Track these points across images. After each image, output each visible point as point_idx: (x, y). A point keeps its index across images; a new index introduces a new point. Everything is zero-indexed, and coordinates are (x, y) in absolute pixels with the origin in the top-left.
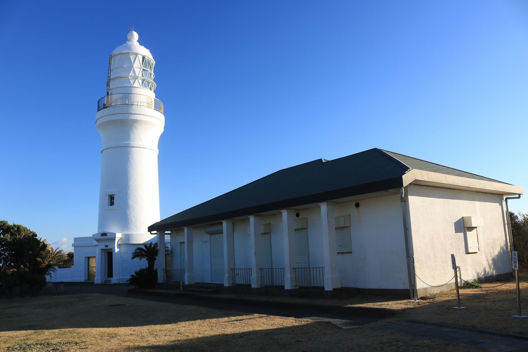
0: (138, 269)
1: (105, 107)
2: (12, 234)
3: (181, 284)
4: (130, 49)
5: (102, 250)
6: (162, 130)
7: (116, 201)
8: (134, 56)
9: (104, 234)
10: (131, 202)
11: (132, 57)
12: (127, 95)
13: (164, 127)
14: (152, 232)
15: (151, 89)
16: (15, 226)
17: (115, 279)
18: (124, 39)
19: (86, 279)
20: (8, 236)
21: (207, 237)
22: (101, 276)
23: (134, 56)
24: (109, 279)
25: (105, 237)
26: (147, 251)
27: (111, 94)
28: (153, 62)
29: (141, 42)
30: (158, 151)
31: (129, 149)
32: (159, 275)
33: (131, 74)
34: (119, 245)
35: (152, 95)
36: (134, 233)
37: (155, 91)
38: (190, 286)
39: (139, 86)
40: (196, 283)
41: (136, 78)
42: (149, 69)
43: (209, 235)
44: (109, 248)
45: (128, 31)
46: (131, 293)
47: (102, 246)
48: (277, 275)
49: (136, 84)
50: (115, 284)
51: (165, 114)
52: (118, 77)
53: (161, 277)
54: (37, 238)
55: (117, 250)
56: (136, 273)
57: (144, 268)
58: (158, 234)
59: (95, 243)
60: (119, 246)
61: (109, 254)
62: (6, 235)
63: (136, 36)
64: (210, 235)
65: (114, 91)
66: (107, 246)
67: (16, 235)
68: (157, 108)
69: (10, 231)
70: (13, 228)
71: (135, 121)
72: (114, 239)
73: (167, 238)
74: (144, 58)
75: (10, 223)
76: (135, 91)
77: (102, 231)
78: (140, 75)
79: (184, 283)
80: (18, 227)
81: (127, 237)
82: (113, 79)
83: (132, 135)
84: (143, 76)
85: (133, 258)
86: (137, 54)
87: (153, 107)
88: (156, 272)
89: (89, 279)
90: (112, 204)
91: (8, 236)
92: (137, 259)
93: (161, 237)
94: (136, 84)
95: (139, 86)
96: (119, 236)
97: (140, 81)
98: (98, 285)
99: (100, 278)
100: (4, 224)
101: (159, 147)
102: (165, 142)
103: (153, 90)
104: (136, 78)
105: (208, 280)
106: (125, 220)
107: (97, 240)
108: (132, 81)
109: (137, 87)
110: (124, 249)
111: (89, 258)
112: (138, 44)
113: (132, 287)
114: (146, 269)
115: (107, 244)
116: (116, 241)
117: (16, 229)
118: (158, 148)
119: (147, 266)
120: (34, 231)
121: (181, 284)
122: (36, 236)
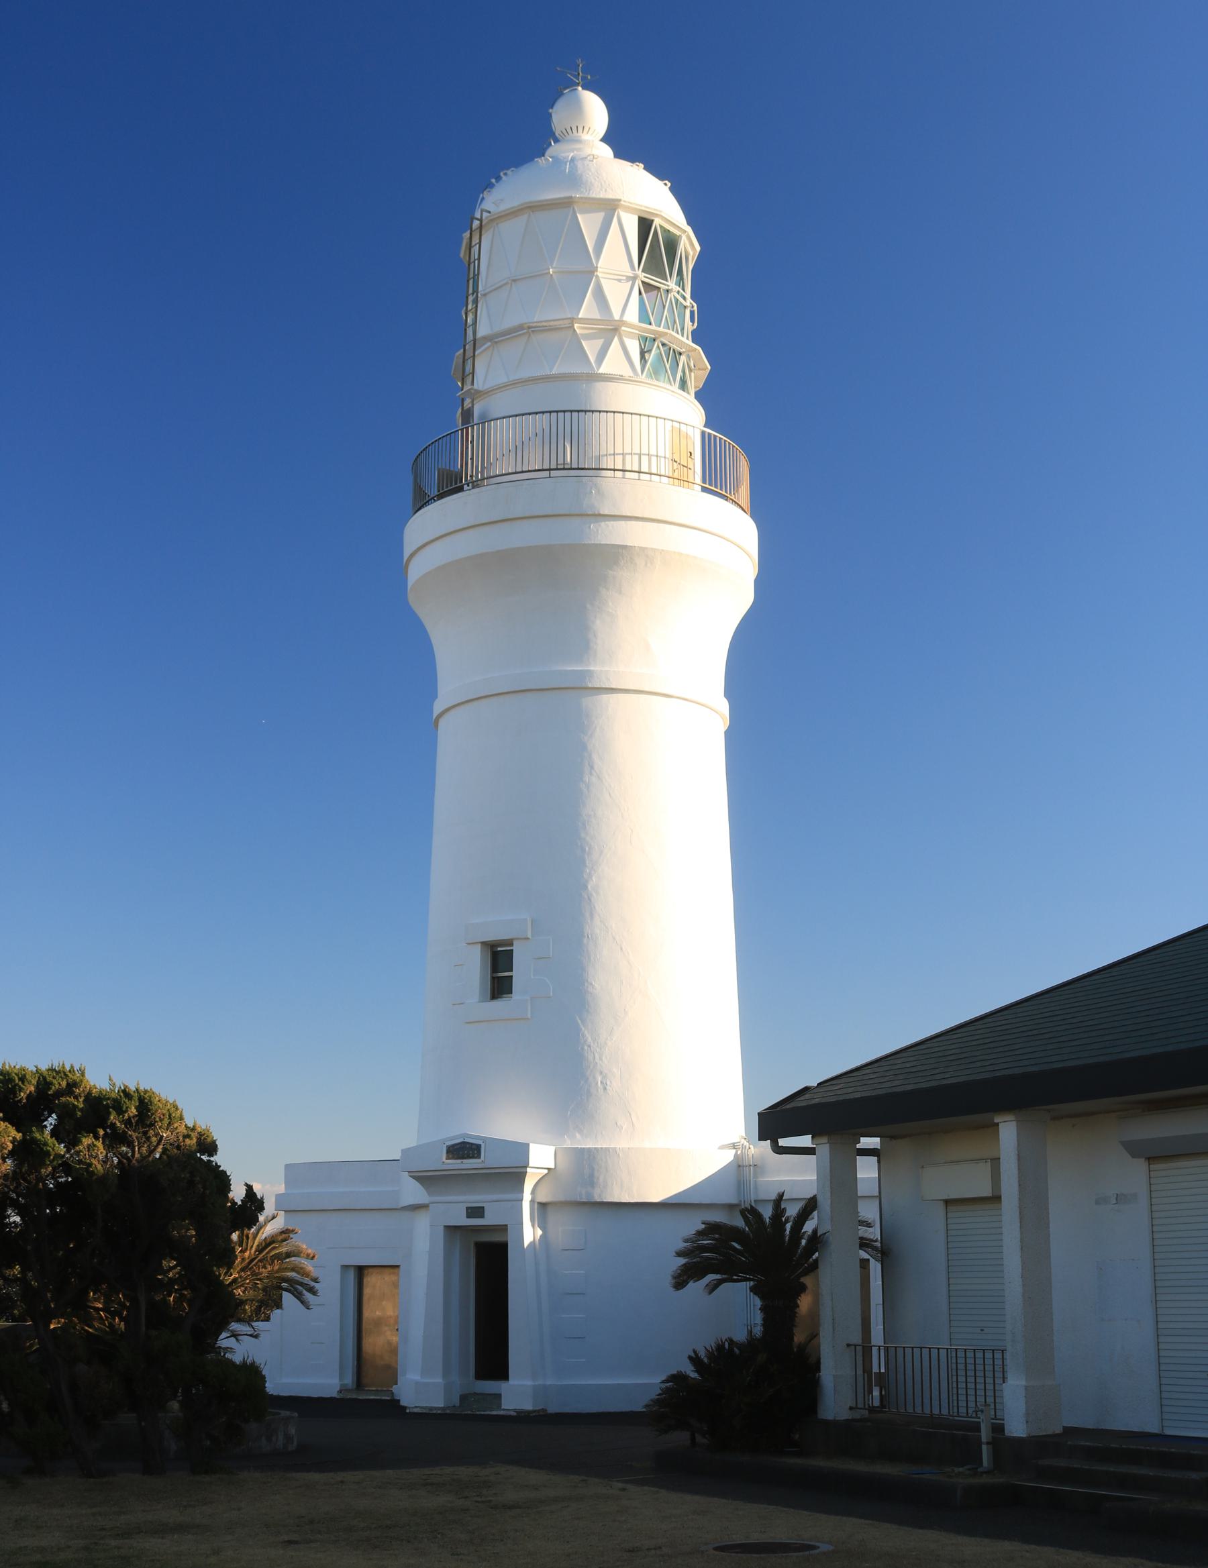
0: (704, 1343)
1: (452, 484)
2: (115, 1139)
3: (985, 1435)
4: (574, 179)
5: (451, 1230)
6: (743, 597)
7: (520, 974)
8: (599, 217)
9: (465, 1150)
10: (600, 981)
11: (588, 224)
12: (568, 419)
13: (758, 582)
14: (783, 1142)
15: (683, 385)
16: (126, 1093)
17: (518, 1392)
18: (533, 137)
19: (349, 1380)
20: (94, 1151)
21: (1133, 1175)
22: (446, 1373)
23: (599, 217)
24: (489, 1386)
25: (474, 1165)
26: (744, 1243)
27: (485, 420)
28: (690, 246)
29: (623, 141)
30: (724, 706)
31: (587, 701)
32: (828, 1374)
33: (588, 309)
34: (543, 1206)
35: (693, 415)
36: (620, 1143)
37: (700, 396)
38: (1040, 1445)
39: (627, 372)
40: (1068, 1431)
41: (610, 330)
42: (672, 284)
43: (1141, 1165)
44: (488, 1220)
45: (556, 88)
46: (674, 1471)
47: (453, 1208)
48: (918, 1378)
49: (613, 363)
50: (522, 1418)
51: (757, 511)
52: (521, 327)
53: (838, 1394)
54: (217, 1159)
55: (530, 1234)
56: (695, 1360)
57: (741, 1336)
58: (824, 1149)
59: (413, 1192)
60: (542, 1209)
61: (487, 1261)
62: (87, 1141)
63: (594, 112)
64: (1151, 1159)
65: (498, 405)
66: (476, 1212)
67: (130, 1144)
68: (715, 480)
69: (102, 1121)
70: (118, 1106)
71: (617, 555)
72: (515, 1176)
73: (867, 1170)
74: (645, 225)
75: (98, 1079)
76: (611, 396)
77: (456, 1131)
78: (632, 315)
79: (998, 1429)
80: (145, 1104)
81: (585, 1165)
82: (486, 339)
83: (599, 625)
84: (644, 316)
85: (680, 1282)
86: (610, 207)
87: (698, 480)
88: (805, 1368)
89: (359, 1384)
90: (500, 987)
91: (94, 1151)
92: (696, 1288)
93: (841, 1177)
94: (613, 363)
95: (627, 372)
96: (541, 1157)
97: (634, 347)
98: (426, 1417)
99: (439, 1380)
100: (72, 1085)
101: (731, 692)
102: (763, 663)
103: (692, 391)
104: (610, 330)
105: (1137, 1415)
106: (569, 1075)
107: (426, 1179)
108: (591, 348)
109: (620, 379)
110: (564, 1227)
111: (361, 1271)
112: (606, 151)
113: (679, 1438)
114: (752, 1345)
115: (475, 1198)
116: (529, 1185)
117: (133, 1111)
118: (729, 693)
119: (758, 1331)
120: (202, 1125)
121: (985, 1435)
122: (212, 1148)
